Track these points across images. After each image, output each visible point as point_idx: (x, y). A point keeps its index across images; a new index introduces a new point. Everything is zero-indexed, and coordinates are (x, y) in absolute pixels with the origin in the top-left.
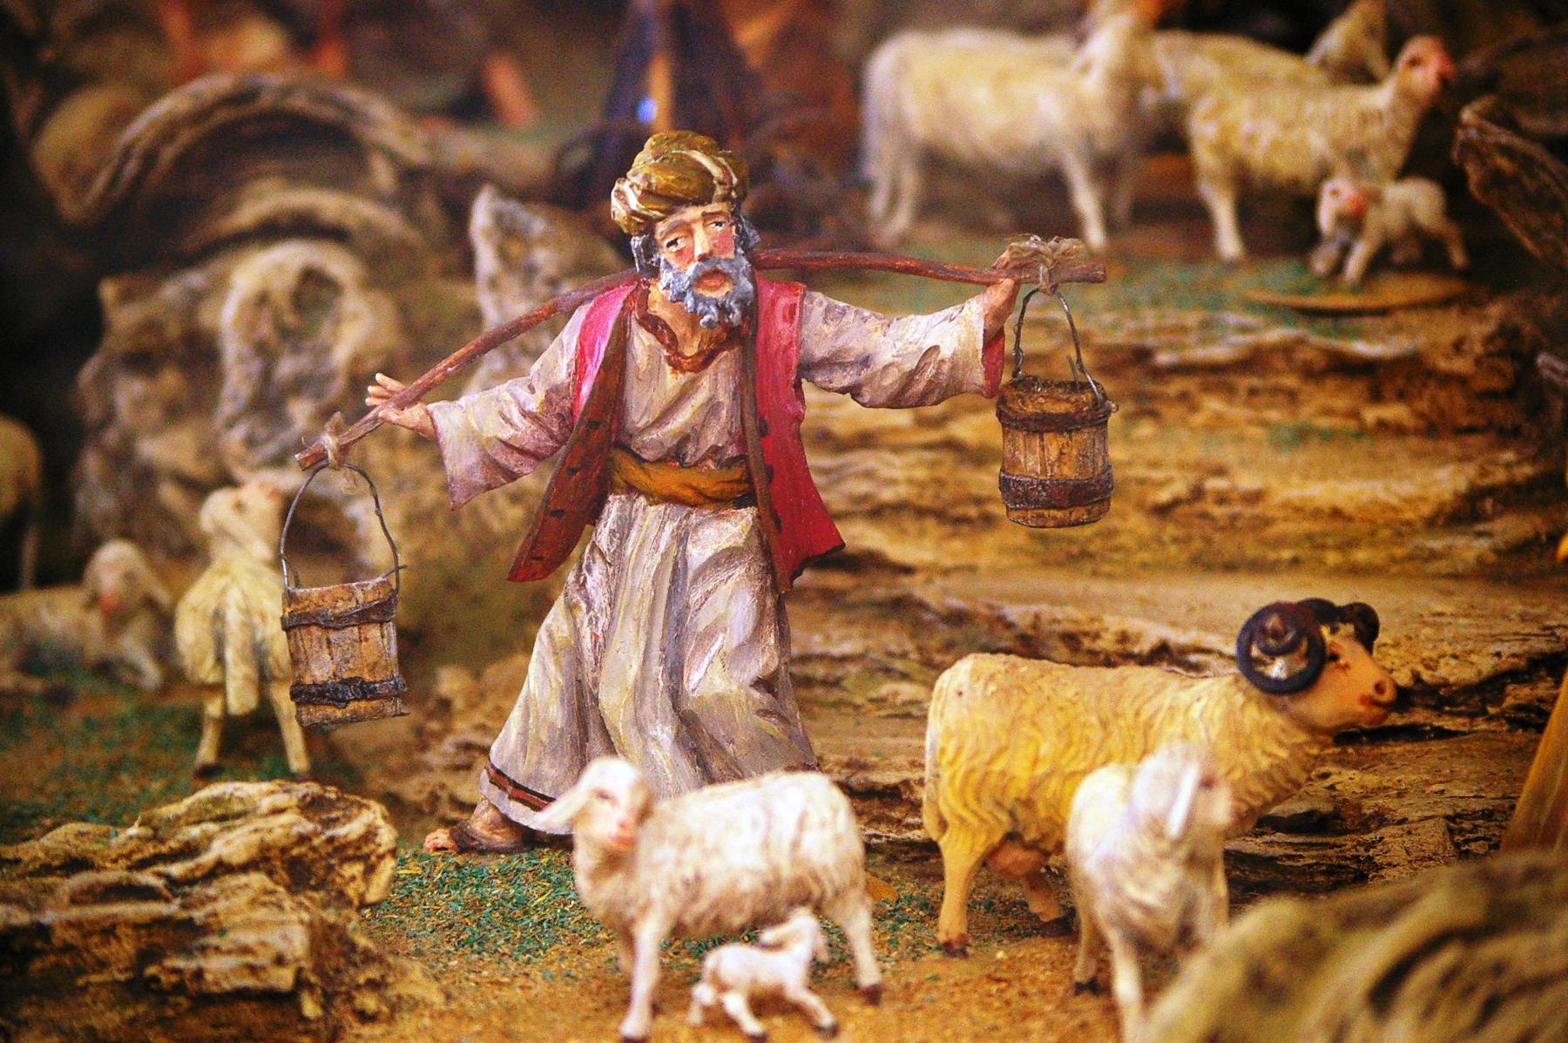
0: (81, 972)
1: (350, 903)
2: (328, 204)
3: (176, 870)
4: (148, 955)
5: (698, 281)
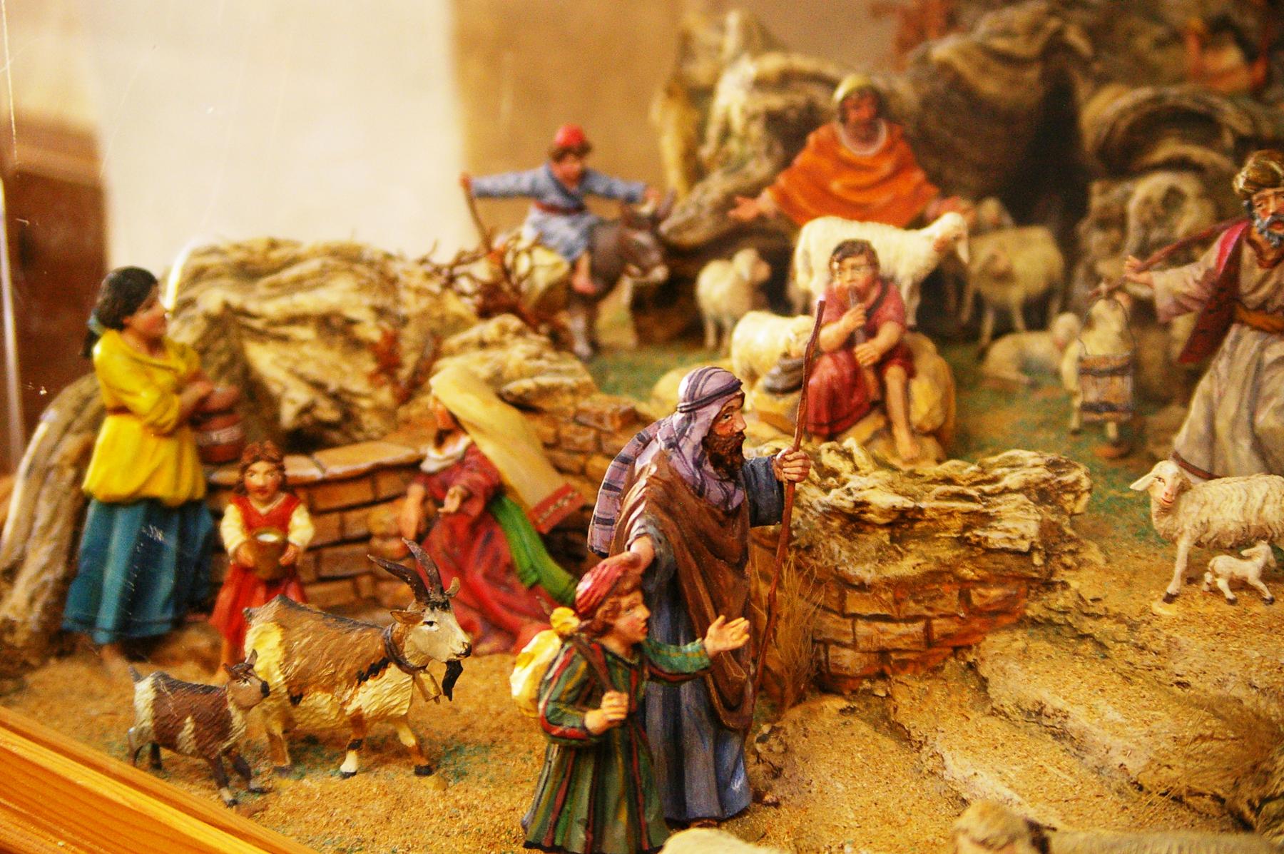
0: (938, 531)
2: (1196, 153)
3: (987, 488)
4: (967, 527)
5: (1271, 225)
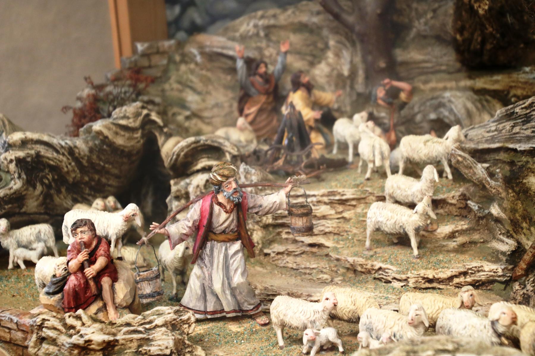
0: (126, 350)
1: (185, 334)
3: (147, 326)
4: (140, 346)
